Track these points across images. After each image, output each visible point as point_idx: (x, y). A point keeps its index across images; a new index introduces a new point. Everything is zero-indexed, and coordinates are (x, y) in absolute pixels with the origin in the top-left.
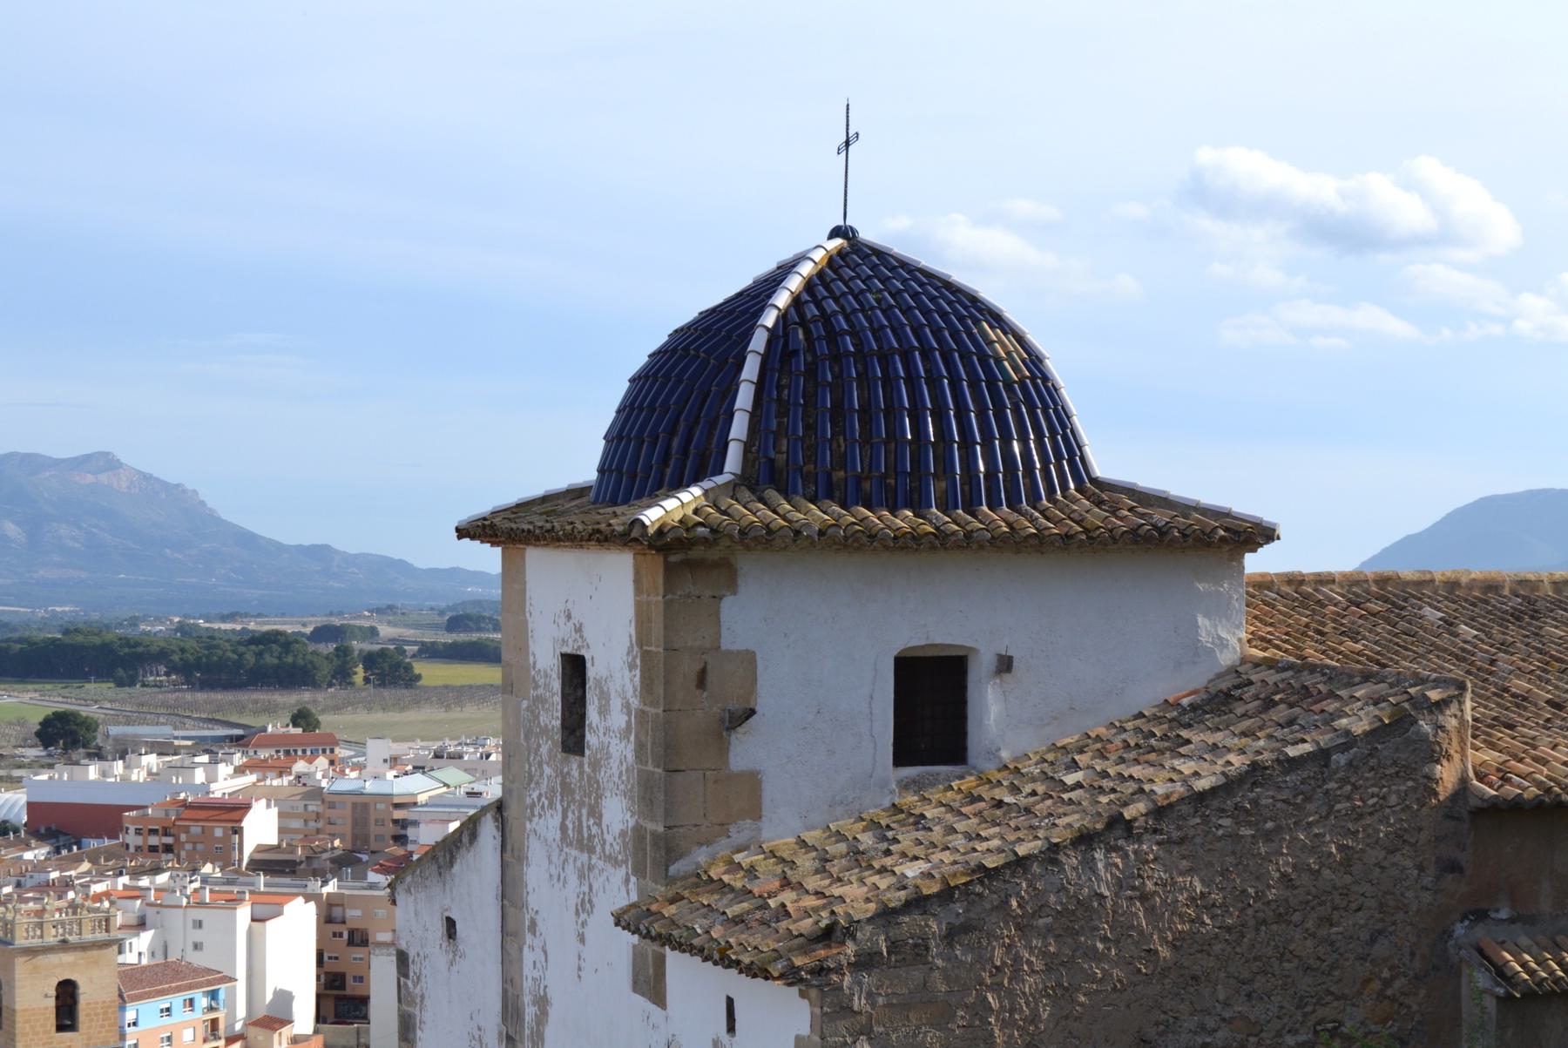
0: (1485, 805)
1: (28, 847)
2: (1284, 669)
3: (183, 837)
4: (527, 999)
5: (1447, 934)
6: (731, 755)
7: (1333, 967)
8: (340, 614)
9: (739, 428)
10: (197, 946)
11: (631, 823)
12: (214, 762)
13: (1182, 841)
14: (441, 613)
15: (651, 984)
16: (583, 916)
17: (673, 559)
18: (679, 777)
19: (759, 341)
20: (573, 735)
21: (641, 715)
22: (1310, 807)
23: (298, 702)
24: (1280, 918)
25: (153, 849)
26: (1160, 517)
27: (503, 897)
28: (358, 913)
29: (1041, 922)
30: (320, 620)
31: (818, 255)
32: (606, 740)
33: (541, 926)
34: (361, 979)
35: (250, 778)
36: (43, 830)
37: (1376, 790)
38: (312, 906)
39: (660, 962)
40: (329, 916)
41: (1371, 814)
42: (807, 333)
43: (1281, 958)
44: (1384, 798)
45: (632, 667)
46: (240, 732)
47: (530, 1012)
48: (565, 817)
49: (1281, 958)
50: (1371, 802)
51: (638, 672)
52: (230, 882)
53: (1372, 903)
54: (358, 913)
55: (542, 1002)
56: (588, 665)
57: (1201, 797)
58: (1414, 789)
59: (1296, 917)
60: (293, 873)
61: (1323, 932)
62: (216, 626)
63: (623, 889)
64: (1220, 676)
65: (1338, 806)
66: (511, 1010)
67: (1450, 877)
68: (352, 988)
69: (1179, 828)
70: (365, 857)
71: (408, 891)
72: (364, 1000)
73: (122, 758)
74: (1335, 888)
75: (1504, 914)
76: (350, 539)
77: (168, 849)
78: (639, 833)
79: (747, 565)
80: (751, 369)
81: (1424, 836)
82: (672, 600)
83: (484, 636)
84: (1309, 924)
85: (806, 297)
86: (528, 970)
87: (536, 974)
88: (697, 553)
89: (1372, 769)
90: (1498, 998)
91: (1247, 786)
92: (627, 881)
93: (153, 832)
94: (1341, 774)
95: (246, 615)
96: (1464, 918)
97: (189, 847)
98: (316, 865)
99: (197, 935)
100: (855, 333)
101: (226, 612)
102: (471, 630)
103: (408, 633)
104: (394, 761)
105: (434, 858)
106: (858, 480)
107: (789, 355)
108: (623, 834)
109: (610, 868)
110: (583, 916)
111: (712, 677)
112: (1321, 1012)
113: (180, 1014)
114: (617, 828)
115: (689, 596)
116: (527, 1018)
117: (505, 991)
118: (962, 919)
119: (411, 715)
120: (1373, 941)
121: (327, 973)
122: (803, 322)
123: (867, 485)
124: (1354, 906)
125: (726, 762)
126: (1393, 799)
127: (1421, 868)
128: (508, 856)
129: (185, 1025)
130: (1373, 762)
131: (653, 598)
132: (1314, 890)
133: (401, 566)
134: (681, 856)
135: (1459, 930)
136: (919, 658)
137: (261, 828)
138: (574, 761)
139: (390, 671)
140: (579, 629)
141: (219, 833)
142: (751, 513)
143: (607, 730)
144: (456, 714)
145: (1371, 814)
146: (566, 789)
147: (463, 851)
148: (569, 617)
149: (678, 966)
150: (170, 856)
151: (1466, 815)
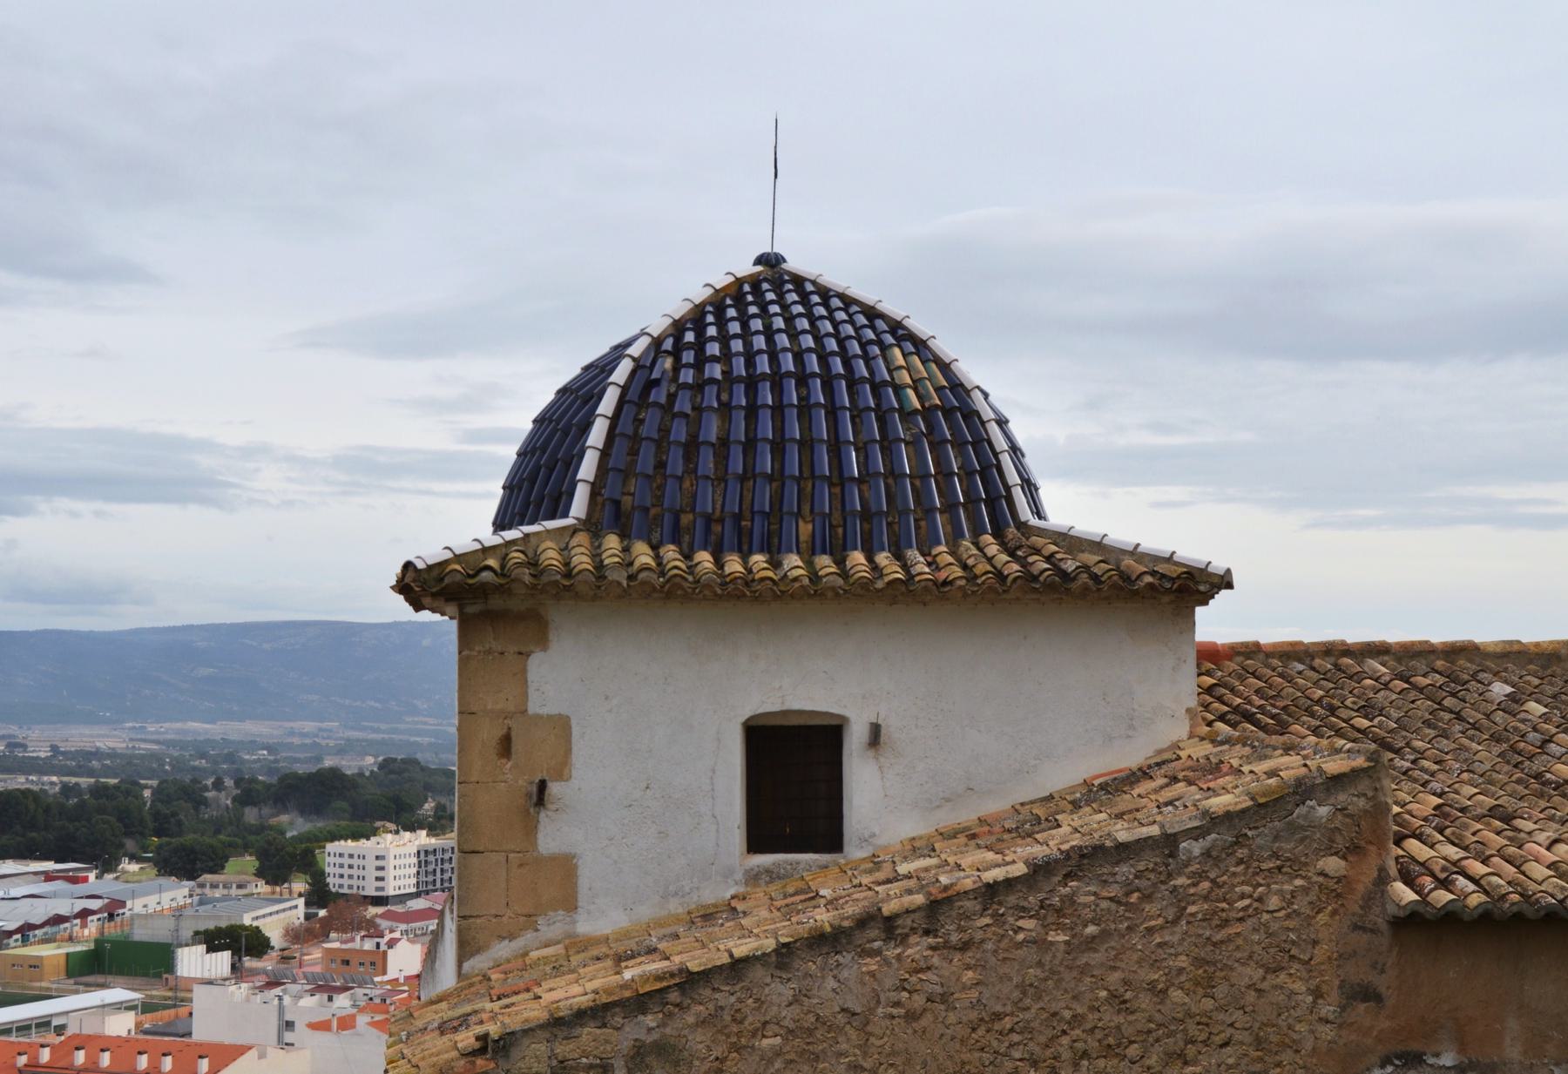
0: (1402, 914)
2: (1222, 743)
6: (540, 836)
17: (470, 609)
18: (475, 859)
22: (1150, 908)
24: (1108, 1051)
37: (1247, 889)
41: (1241, 920)
44: (1260, 900)
50: (1240, 904)
53: (1245, 1037)
57: (991, 892)
58: (1305, 890)
59: (1133, 1051)
65: (1192, 909)
67: (1362, 1007)
69: (961, 929)
74: (1189, 1015)
79: (556, 615)
81: (1320, 953)
82: (468, 657)
88: (496, 602)
89: (1240, 862)
91: (1056, 879)
94: (1194, 867)
111: (517, 746)
115: (489, 652)
118: (655, 1036)
124: (1218, 1040)
125: (534, 844)
126: (1274, 902)
127: (1317, 994)
130: (1241, 853)
132: (1158, 1017)
134: (478, 951)
136: (773, 728)
145: (1241, 920)
151: (1384, 926)
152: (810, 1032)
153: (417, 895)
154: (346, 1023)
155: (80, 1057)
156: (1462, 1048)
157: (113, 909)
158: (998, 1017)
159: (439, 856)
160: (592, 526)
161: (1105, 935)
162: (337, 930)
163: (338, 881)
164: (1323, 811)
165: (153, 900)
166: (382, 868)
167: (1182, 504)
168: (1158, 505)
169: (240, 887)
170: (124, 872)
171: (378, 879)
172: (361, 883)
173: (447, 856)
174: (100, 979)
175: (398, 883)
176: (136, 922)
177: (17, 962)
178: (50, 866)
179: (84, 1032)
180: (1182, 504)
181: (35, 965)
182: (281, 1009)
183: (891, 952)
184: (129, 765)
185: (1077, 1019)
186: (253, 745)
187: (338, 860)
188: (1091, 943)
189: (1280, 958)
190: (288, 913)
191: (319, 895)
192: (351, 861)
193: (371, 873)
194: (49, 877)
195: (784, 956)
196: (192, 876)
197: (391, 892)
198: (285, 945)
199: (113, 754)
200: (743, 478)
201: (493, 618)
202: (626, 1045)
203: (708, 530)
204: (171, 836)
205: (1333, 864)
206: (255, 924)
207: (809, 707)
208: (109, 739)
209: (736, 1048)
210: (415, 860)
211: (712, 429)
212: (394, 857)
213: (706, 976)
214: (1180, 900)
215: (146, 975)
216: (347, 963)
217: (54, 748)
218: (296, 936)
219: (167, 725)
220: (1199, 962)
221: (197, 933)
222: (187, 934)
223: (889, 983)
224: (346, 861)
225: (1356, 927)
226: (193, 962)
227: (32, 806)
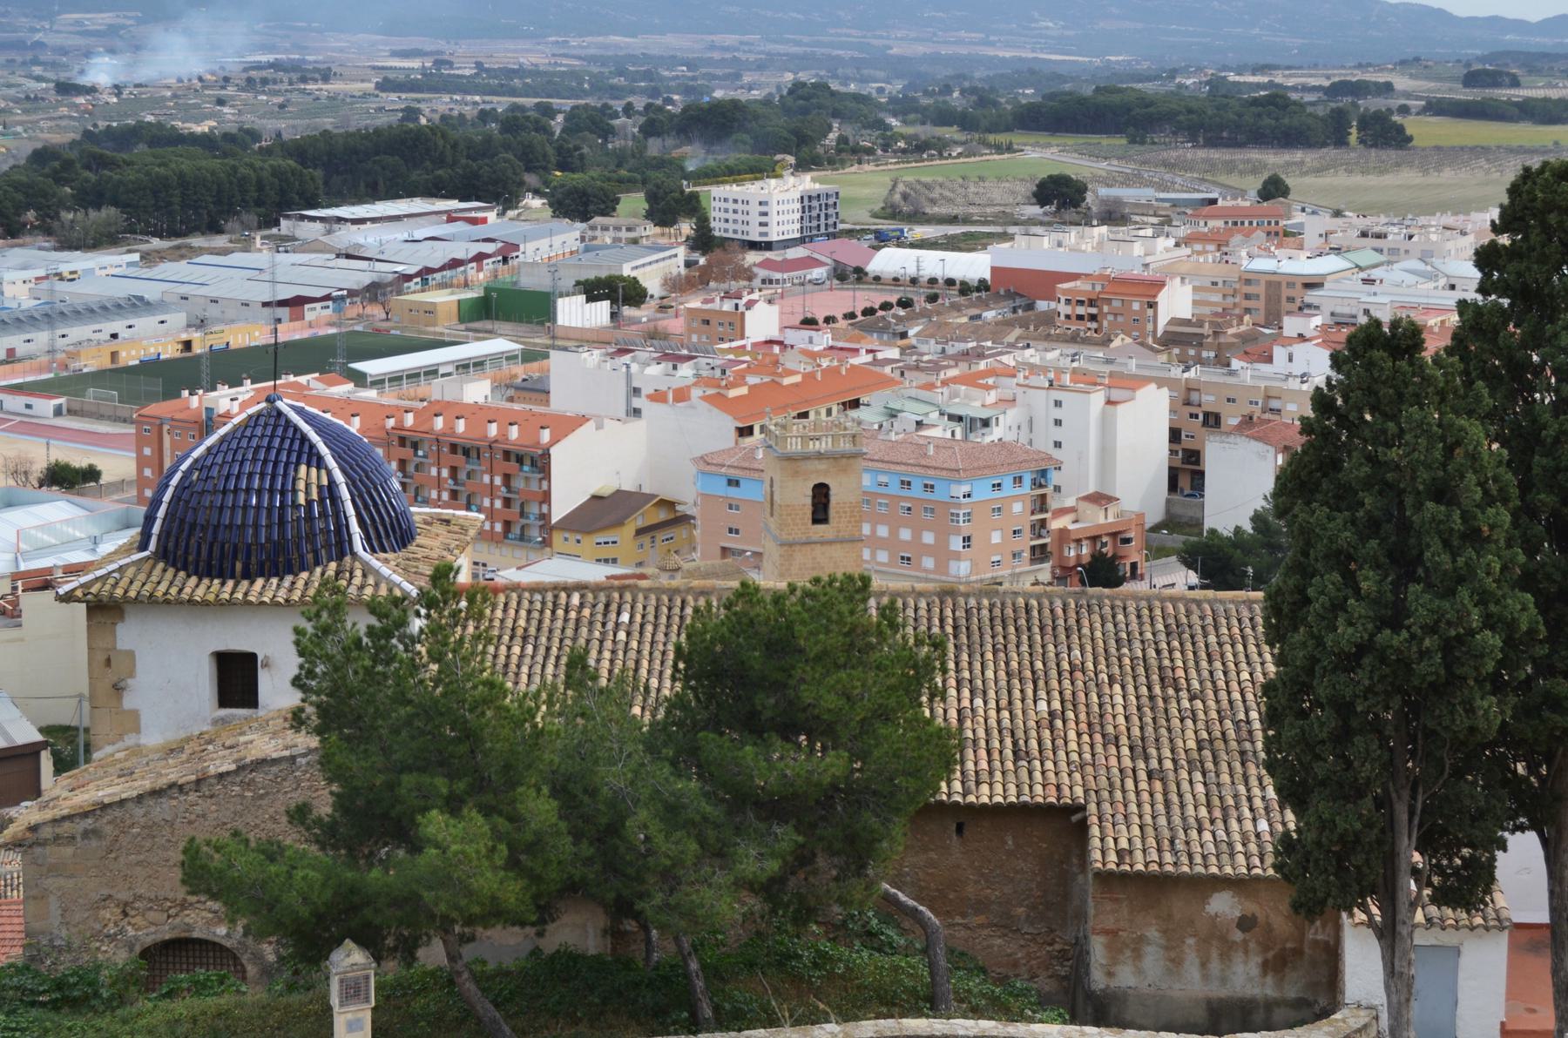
1: (989, 308)
3: (1106, 309)
25: (1080, 317)
28: (1212, 398)
35: (1185, 251)
36: (1002, 292)
38: (1165, 392)
40: (1186, 398)
54: (1212, 398)
57: (221, 776)
77: (1093, 318)
93: (1081, 303)
95: (1276, 67)
97: (1111, 318)
101: (1262, 62)
113: (1009, 489)
129: (1016, 498)
141: (1136, 306)
153: (801, 241)
154: (681, 395)
155: (439, 423)
157: (507, 253)
159: (823, 202)
161: (267, 794)
162: (716, 279)
163: (724, 225)
165: (544, 242)
166: (765, 214)
169: (629, 229)
170: (527, 208)
171: (761, 224)
172: (745, 228)
173: (831, 201)
174: (488, 325)
175: (781, 228)
176: (523, 270)
177: (412, 308)
178: (454, 204)
179: (447, 398)
181: (430, 311)
182: (629, 376)
183: (182, 798)
184: (549, 82)
185: (256, 826)
186: (672, 61)
187: (723, 205)
188: (261, 797)
190: (668, 262)
191: (704, 241)
192: (736, 206)
193: (755, 219)
194: (451, 218)
195: (140, 798)
196: (585, 218)
197: (774, 237)
198: (664, 294)
199: (535, 72)
204: (573, 171)
206: (633, 274)
208: (532, 56)
210: (798, 206)
211: (247, 468)
212: (775, 201)
214: (298, 781)
215: (529, 322)
216: (708, 322)
217: (479, 65)
218: (678, 286)
219: (589, 39)
221: (578, 283)
222: (568, 283)
224: (731, 206)
226: (574, 312)
227: (441, 143)
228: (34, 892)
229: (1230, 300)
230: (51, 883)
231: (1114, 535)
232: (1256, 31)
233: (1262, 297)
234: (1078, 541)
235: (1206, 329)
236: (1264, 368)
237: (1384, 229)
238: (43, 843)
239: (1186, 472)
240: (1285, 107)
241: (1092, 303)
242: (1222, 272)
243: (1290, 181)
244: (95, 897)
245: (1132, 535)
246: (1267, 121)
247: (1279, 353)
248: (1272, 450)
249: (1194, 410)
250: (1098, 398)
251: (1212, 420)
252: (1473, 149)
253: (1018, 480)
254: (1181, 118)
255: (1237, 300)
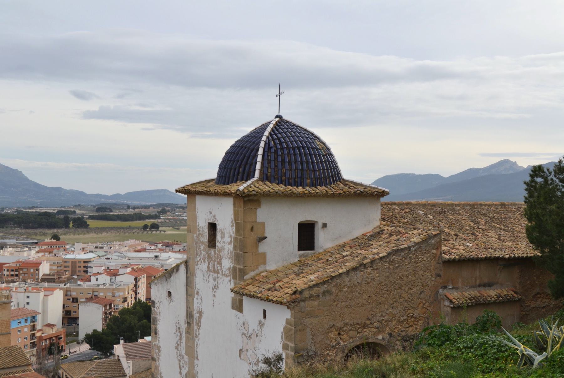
3: (21, 272)
4: (195, 312)
5: (438, 292)
7: (412, 300)
8: (64, 207)
9: (258, 166)
10: (28, 303)
11: (232, 266)
12: (30, 250)
13: (377, 269)
14: (94, 207)
15: (238, 306)
16: (215, 290)
17: (246, 199)
19: (262, 144)
20: (212, 242)
21: (235, 239)
22: (406, 261)
23: (53, 233)
24: (400, 288)
25: (12, 275)
26: (362, 189)
27: (187, 285)
28: (75, 293)
29: (345, 289)
30: (59, 209)
31: (274, 122)
32: (223, 245)
33: (200, 293)
34: (75, 312)
35: (41, 254)
38: (62, 291)
39: (241, 302)
40: (66, 294)
42: (274, 142)
43: (400, 298)
45: (232, 226)
46: (36, 241)
47: (196, 316)
48: (209, 264)
49: (400, 298)
51: (234, 228)
52: (37, 285)
53: (421, 284)
55: (200, 313)
56: (217, 225)
57: (381, 258)
59: (403, 288)
60: (54, 282)
61: (409, 292)
62: (27, 210)
63: (229, 283)
64: (375, 228)
66: (189, 315)
68: (73, 315)
70: (75, 277)
71: (156, 284)
72: (77, 318)
73: (2, 249)
75: (450, 287)
76: (68, 185)
77: (17, 275)
78: (234, 269)
79: (263, 200)
80: (261, 151)
81: (432, 268)
83: (107, 213)
84: (406, 290)
85: (272, 133)
86: (195, 304)
87: (198, 305)
88: (251, 198)
90: (451, 308)
92: (230, 280)
93: (12, 271)
95: (37, 207)
96: (441, 288)
97: (23, 275)
98: (61, 279)
99: (28, 300)
100: (286, 142)
102: (104, 212)
103: (84, 212)
104: (83, 249)
105: (164, 275)
106: (289, 179)
107: (270, 148)
108: (229, 269)
109: (224, 278)
110: (215, 290)
111: (255, 229)
112: (409, 311)
113: (23, 324)
114: (227, 267)
116: (195, 317)
117: (187, 311)
119: (87, 236)
120: (421, 294)
121: (66, 311)
122: (273, 140)
123: (291, 181)
125: (258, 250)
126: (425, 259)
127: (432, 276)
128: (189, 275)
129: (25, 326)
130: (420, 250)
131: (240, 209)
133: (82, 193)
135: (440, 291)
137: (45, 269)
138: (212, 251)
139: (81, 224)
140: (214, 216)
141: (32, 270)
142: (265, 187)
143: (224, 242)
144: (100, 235)
146: (209, 257)
147: (174, 274)
148: (211, 213)
149: (246, 301)
150: (17, 277)
152: (352, 287)
156: (453, 285)
158: (382, 282)
160: (261, 179)
164: (433, 241)
167: (151, 129)
168: (143, 129)
180: (151, 129)
183: (365, 271)
188: (397, 268)
189: (426, 269)
195: (348, 272)
200: (295, 170)
201: (250, 201)
202: (322, 291)
203: (289, 181)
205: (434, 251)
207: (311, 219)
209: (340, 291)
213: (335, 277)
214: (411, 259)
220: (413, 270)
223: (365, 277)
225: (437, 263)
228: (300, 327)
229: (59, 268)
230: (307, 321)
231: (56, 337)
232: (26, 197)
233: (70, 267)
234: (45, 340)
235: (56, 277)
236: (87, 283)
237: (102, 246)
238: (304, 300)
239: (70, 318)
240: (50, 216)
241: (16, 270)
242: (55, 259)
243: (61, 237)
244: (327, 326)
245: (62, 336)
246: (44, 220)
247: (93, 279)
248: (102, 306)
249: (69, 298)
250: (42, 294)
251: (75, 300)
252: (107, 228)
253: (26, 320)
254: (16, 220)
255: (62, 268)
